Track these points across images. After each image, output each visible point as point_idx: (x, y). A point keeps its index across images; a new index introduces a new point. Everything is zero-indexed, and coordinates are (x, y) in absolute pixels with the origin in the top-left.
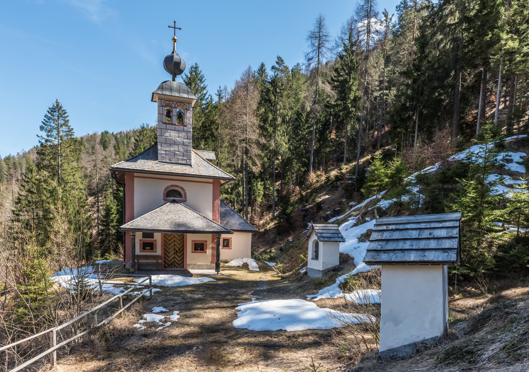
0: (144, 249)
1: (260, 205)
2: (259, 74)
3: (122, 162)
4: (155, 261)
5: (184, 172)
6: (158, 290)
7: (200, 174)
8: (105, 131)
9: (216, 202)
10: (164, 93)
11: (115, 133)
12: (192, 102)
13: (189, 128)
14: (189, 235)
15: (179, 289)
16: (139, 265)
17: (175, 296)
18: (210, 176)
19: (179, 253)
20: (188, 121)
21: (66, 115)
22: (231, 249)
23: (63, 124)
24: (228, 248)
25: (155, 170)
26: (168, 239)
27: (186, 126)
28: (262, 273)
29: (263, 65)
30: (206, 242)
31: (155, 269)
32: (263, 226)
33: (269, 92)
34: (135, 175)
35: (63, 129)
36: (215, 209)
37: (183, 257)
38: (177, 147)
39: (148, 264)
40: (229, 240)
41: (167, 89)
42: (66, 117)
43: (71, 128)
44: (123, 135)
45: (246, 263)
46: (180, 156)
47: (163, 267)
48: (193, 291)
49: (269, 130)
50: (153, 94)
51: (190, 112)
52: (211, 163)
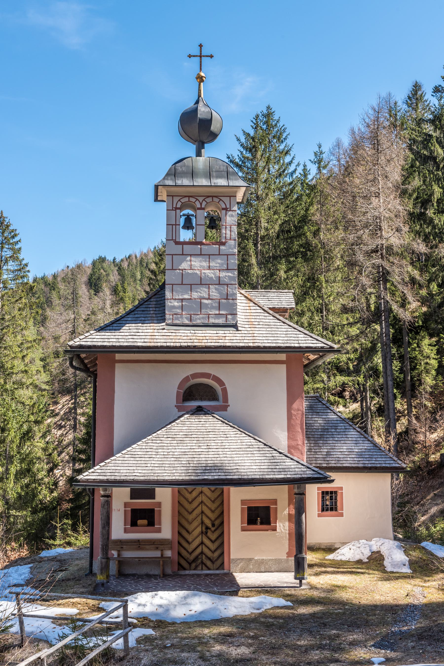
0: (134, 524)
1: (431, 394)
2: (409, 106)
3: (92, 332)
4: (158, 554)
5: (221, 343)
6: (149, 632)
7: (256, 345)
8: (100, 258)
9: (295, 406)
10: (179, 182)
11: (118, 260)
12: (236, 192)
13: (230, 248)
14: (233, 490)
15: (198, 631)
16: (121, 563)
17: (182, 651)
18: (279, 347)
19: (213, 532)
20: (228, 232)
21: (16, 239)
22: (341, 515)
23: (11, 257)
24: (334, 513)
25: (159, 344)
26: (187, 500)
27: (224, 244)
28: (417, 581)
29: (417, 87)
30: (275, 502)
31: (157, 571)
32: (436, 446)
33: (429, 141)
34: (117, 358)
35: (9, 267)
36: (292, 422)
37: (223, 543)
38: (207, 290)
39: (142, 561)
40: (336, 492)
41: (183, 174)
42: (17, 243)
43: (24, 262)
44: (134, 261)
45: (379, 552)
46: (213, 308)
47: (176, 567)
48: (231, 635)
49: (436, 221)
50: (156, 187)
51: (233, 213)
52: (281, 318)
